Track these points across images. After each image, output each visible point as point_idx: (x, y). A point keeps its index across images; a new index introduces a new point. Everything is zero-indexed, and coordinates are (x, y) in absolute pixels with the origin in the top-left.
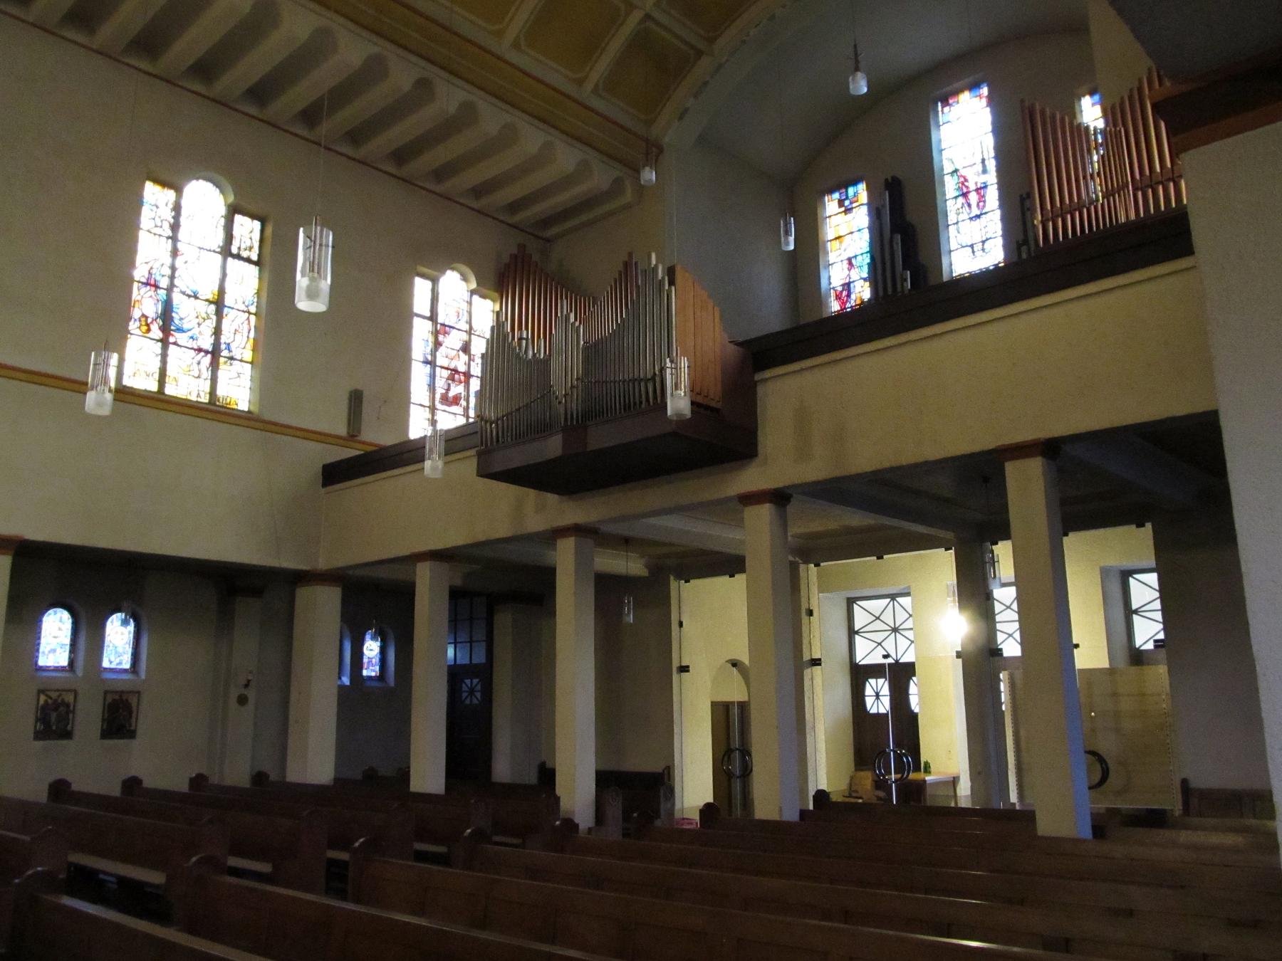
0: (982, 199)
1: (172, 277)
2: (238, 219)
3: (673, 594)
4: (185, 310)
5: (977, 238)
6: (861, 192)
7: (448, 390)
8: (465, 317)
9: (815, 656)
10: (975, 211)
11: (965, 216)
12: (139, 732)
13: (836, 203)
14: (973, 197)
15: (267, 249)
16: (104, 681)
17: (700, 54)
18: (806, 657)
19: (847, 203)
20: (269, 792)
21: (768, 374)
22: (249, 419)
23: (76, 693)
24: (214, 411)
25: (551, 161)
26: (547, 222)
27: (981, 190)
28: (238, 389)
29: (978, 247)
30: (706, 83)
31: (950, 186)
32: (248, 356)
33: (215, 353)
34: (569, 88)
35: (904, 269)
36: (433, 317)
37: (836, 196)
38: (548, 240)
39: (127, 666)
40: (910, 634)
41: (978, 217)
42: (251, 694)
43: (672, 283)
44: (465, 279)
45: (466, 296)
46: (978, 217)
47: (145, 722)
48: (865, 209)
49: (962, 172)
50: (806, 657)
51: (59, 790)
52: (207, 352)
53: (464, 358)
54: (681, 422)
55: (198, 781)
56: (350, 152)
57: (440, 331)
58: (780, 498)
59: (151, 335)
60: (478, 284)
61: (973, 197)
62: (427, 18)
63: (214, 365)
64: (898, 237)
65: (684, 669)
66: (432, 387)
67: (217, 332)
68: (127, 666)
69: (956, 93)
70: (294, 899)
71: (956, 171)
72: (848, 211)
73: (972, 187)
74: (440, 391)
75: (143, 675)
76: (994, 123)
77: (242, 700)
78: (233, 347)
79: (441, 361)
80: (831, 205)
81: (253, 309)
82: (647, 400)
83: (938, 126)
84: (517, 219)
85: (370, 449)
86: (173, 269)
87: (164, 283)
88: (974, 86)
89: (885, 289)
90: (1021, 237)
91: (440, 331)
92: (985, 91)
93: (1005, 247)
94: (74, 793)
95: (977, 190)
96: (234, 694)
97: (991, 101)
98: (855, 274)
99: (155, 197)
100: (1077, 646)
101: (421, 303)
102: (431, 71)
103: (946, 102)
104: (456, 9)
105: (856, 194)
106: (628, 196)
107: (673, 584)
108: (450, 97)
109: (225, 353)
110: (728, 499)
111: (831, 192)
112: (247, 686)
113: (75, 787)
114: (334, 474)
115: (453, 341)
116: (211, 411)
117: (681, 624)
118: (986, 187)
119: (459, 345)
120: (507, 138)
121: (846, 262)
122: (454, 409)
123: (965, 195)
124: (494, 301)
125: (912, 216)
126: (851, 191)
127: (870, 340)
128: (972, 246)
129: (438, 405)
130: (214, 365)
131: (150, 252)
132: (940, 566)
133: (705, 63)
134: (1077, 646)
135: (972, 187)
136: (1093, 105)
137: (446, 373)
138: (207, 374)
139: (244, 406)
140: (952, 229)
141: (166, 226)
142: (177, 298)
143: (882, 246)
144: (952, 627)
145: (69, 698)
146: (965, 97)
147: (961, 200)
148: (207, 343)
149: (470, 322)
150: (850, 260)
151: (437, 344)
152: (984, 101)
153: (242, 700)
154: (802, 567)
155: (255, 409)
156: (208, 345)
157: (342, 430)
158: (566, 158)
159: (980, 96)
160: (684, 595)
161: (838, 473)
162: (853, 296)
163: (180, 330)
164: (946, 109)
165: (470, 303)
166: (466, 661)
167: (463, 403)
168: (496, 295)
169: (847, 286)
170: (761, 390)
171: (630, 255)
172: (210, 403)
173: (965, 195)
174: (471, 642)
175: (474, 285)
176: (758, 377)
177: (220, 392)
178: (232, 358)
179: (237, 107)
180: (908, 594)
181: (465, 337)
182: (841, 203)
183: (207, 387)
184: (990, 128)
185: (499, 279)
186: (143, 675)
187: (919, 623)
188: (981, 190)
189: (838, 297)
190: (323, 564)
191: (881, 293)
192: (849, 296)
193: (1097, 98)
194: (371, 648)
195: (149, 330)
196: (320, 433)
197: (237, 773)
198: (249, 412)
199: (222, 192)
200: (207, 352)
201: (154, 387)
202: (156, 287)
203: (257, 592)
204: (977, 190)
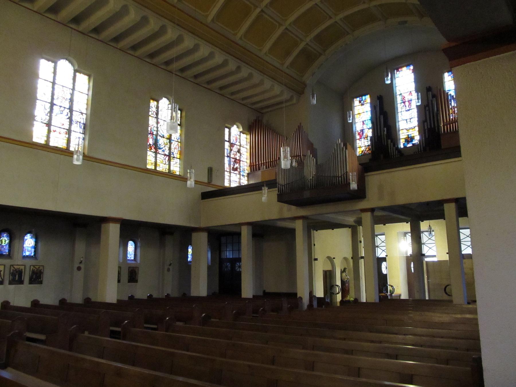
0: (410, 104)
1: (157, 131)
2: (77, 74)
3: (312, 234)
4: (162, 141)
5: (408, 118)
6: (367, 98)
7: (234, 166)
8: (238, 141)
9: (316, 257)
10: (408, 108)
11: (404, 109)
12: (139, 280)
13: (358, 102)
14: (407, 104)
15: (183, 120)
16: (128, 264)
17: (321, 54)
18: (360, 256)
19: (362, 102)
20: (89, 304)
21: (369, 174)
22: (56, 150)
23: (25, 266)
24: (170, 175)
25: (273, 90)
26: (262, 108)
27: (410, 101)
28: (176, 168)
29: (408, 121)
30: (322, 64)
31: (399, 99)
32: (178, 156)
33: (169, 156)
34: (277, 65)
35: (384, 127)
36: (229, 141)
37: (358, 99)
38: (263, 113)
39: (133, 258)
40: (384, 248)
41: (409, 110)
42: (171, 267)
43: (346, 149)
44: (238, 127)
45: (239, 133)
46: (409, 110)
47: (141, 276)
48: (369, 105)
49: (403, 95)
50: (360, 256)
51: (35, 303)
52: (167, 156)
53: (238, 154)
54: (354, 191)
55: (63, 302)
56: (180, 75)
57: (232, 145)
58: (372, 210)
59: (152, 150)
60: (78, 67)
61: (407, 104)
62: (221, 35)
63: (169, 160)
64: (382, 117)
65: (316, 259)
66: (230, 165)
67: (170, 149)
68: (133, 258)
69: (402, 67)
70: (120, 343)
71: (401, 94)
72: (362, 105)
73: (407, 100)
74: (232, 166)
75: (139, 262)
76: (415, 79)
77: (79, 269)
78: (174, 153)
79: (232, 156)
80: (356, 102)
81: (179, 141)
82: (342, 182)
83: (395, 78)
84: (254, 107)
85: (221, 188)
86: (157, 128)
87: (155, 133)
88: (408, 65)
89: (377, 133)
90: (424, 119)
91: (232, 145)
92: (412, 67)
93: (418, 121)
94: (42, 305)
95: (408, 101)
96: (166, 268)
97: (414, 71)
98: (365, 127)
99: (45, 67)
100: (447, 253)
102: (166, 22)
103: (398, 70)
104: (197, 10)
105: (365, 99)
106: (294, 101)
107: (312, 231)
108: (245, 72)
109: (172, 156)
110: (356, 210)
111: (357, 97)
112: (170, 265)
113: (41, 302)
114: (206, 196)
115: (235, 149)
117: (314, 245)
118: (411, 100)
119: (236, 150)
120: (261, 83)
121: (362, 123)
122: (236, 172)
123: (404, 102)
124: (246, 135)
125: (386, 108)
126: (364, 98)
127: (404, 166)
128: (406, 120)
129: (232, 171)
130: (169, 160)
131: (43, 90)
132: (406, 227)
133: (322, 58)
134: (447, 253)
135: (407, 100)
136: (449, 76)
137: (233, 160)
138: (167, 163)
139: (178, 173)
140: (399, 114)
141: (155, 113)
142: (159, 137)
143: (376, 119)
144: (405, 246)
145: (41, 268)
146: (404, 69)
147: (403, 104)
148: (167, 152)
149: (240, 142)
150: (363, 122)
151: (231, 150)
152: (411, 71)
153: (169, 270)
154: (358, 227)
155: (182, 174)
156: (167, 154)
157: (206, 180)
158: (277, 89)
159: (410, 69)
160: (315, 235)
161: (392, 204)
162: (364, 134)
163: (160, 149)
164: (398, 73)
165: (240, 136)
167: (239, 170)
168: (248, 133)
169: (362, 131)
170: (366, 179)
171: (301, 123)
172: (169, 172)
173: (404, 102)
174: (233, 250)
175: (241, 130)
176: (366, 174)
177: (172, 169)
178: (174, 157)
179: (69, 25)
180: (384, 235)
181: (238, 147)
182: (360, 102)
183: (167, 167)
184: (413, 80)
185: (249, 128)
186: (139, 262)
187: (395, 245)
188: (410, 101)
189: (359, 134)
190: (203, 225)
191: (376, 135)
192: (363, 134)
193: (450, 73)
194: (131, 247)
195: (151, 149)
196: (140, 169)
197: (77, 298)
198: (179, 175)
199: (72, 64)
200: (167, 156)
201: (153, 168)
202: (153, 134)
203: (172, 234)
204: (408, 101)
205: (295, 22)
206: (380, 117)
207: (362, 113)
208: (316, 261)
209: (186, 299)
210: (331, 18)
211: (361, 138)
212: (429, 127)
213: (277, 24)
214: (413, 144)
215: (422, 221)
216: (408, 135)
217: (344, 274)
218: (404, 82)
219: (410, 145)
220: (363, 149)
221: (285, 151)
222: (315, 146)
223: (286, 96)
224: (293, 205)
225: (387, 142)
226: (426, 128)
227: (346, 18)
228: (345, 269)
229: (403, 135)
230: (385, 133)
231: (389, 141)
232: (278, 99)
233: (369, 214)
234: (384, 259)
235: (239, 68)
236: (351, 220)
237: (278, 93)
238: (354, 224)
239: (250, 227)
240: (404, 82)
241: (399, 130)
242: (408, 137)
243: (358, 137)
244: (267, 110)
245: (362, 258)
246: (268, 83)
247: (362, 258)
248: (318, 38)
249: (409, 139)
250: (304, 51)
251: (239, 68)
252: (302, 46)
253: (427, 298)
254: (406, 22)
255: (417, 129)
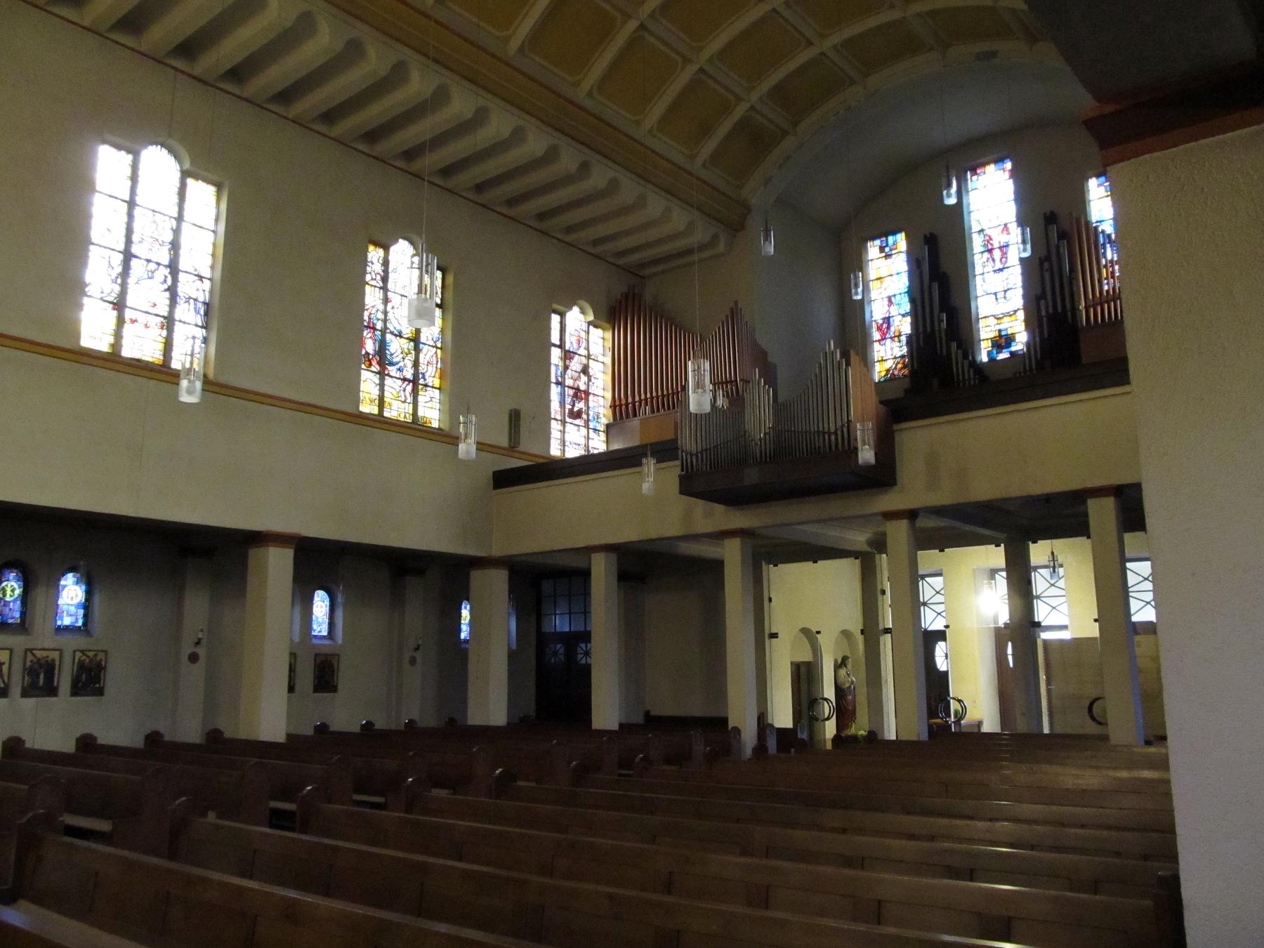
0: (1004, 255)
1: (385, 321)
2: (190, 181)
3: (764, 573)
4: (396, 346)
5: (1000, 288)
6: (900, 241)
7: (573, 406)
8: (584, 345)
9: (774, 631)
10: (998, 265)
11: (989, 268)
12: (339, 687)
13: (877, 249)
14: (997, 254)
15: (449, 294)
16: (314, 646)
17: (785, 133)
18: (881, 627)
19: (887, 249)
20: (218, 745)
21: (904, 425)
22: (138, 367)
23: (61, 651)
24: (416, 428)
25: (668, 220)
26: (643, 265)
27: (1004, 248)
28: (431, 411)
29: (1000, 295)
30: (789, 157)
31: (977, 243)
32: (437, 383)
33: (414, 382)
34: (680, 159)
35: (941, 311)
36: (561, 346)
37: (878, 242)
38: (643, 278)
39: (325, 633)
40: (940, 608)
41: (1001, 270)
42: (418, 655)
43: (848, 364)
45: (585, 326)
46: (1001, 270)
47: (345, 677)
48: (903, 257)
49: (988, 232)
50: (881, 627)
51: (86, 743)
52: (409, 381)
53: (584, 378)
54: (868, 468)
55: (153, 739)
56: (441, 183)
57: (568, 355)
58: (912, 515)
59: (373, 369)
60: (192, 164)
61: (997, 254)
62: (541, 85)
63: (415, 393)
64: (936, 286)
65: (774, 636)
66: (562, 404)
67: (416, 364)
68: (325, 633)
69: (984, 165)
71: (982, 231)
72: (888, 256)
73: (996, 245)
74: (568, 406)
75: (340, 641)
76: (1017, 193)
77: (194, 658)
78: (427, 375)
79: (569, 382)
80: (873, 249)
81: (439, 345)
83: (968, 192)
84: (621, 262)
85: (541, 461)
86: (385, 313)
87: (379, 325)
88: (999, 160)
89: (925, 326)
90: (1039, 292)
91: (568, 355)
92: (1008, 165)
93: (1024, 296)
94: (103, 746)
95: (1000, 248)
96: (407, 655)
97: (1014, 174)
98: (894, 311)
99: (109, 164)
100: (1096, 620)
101: (375, 267)
102: (407, 54)
103: (974, 172)
104: (482, 24)
105: (895, 243)
106: (721, 247)
107: (764, 567)
108: (600, 176)
109: (421, 381)
110: (872, 515)
111: (873, 239)
112: (417, 649)
113: (101, 741)
114: (504, 479)
115: (576, 364)
116: (380, 422)
117: (770, 600)
118: (1007, 246)
119: (579, 368)
120: (640, 203)
121: (886, 301)
122: (577, 422)
123: (990, 251)
124: (604, 329)
125: (946, 265)
126: (891, 239)
127: (990, 406)
128: (995, 294)
129: (568, 420)
130: (415, 393)
132: (995, 556)
133: (789, 143)
134: (1096, 620)
135: (996, 245)
136: (1099, 185)
137: (571, 392)
138: (410, 399)
139: (435, 425)
140: (979, 279)
141: (378, 278)
142: (389, 337)
143: (922, 291)
144: (992, 603)
145: (101, 656)
146: (991, 168)
147: (986, 255)
148: (409, 374)
149: (587, 349)
150: (889, 298)
151: (566, 368)
152: (1007, 175)
153: (413, 661)
154: (877, 556)
155: (445, 427)
156: (409, 376)
157: (504, 442)
158: (679, 218)
159: (1004, 170)
160: (772, 576)
161: (961, 500)
162: (892, 329)
163: (392, 364)
164: (975, 178)
165: (588, 333)
166: (567, 630)
167: (584, 416)
168: (608, 326)
169: (887, 320)
170: (897, 437)
171: (736, 302)
172: (413, 422)
173: (990, 251)
174: (570, 613)
175: (591, 318)
176: (895, 427)
177: (420, 413)
178: (426, 385)
179: (168, 62)
180: (940, 575)
181: (584, 361)
182: (882, 249)
183: (410, 409)
184: (1012, 197)
185: (611, 314)
186: (340, 641)
187: (967, 599)
188: (1004, 248)
189: (879, 328)
190: (497, 551)
191: (921, 330)
192: (888, 328)
193: (1103, 179)
194: (321, 604)
195: (371, 365)
196: (343, 413)
197: (190, 730)
198: (439, 429)
199: (177, 158)
200: (409, 381)
201: (375, 411)
202: (374, 329)
203: (420, 572)
204: (1000, 248)
205: (723, 54)
206: (930, 288)
207: (887, 277)
208: (774, 640)
209: (456, 732)
210: (810, 43)
211: (884, 338)
212: (1051, 311)
213: (680, 60)
214: (1011, 353)
215: (1035, 542)
216: (1000, 331)
217: (843, 672)
218: (991, 201)
219: (1004, 355)
220: (890, 364)
221: (697, 371)
222: (772, 358)
223: (700, 235)
224: (719, 502)
225: (949, 348)
226: (1044, 313)
227: (848, 43)
228: (845, 659)
229: (986, 332)
230: (944, 325)
231: (954, 345)
232: (681, 244)
233: (903, 524)
234: (941, 635)
235: (585, 167)
236: (859, 538)
237: (682, 228)
238: (866, 548)
239: (613, 557)
240: (991, 201)
241: (978, 319)
242: (1000, 336)
243: (876, 335)
244: (653, 270)
245: (887, 631)
246: (656, 204)
247: (887, 631)
248: (780, 93)
249: (1002, 341)
250: (744, 125)
251: (585, 167)
252: (739, 112)
253: (1046, 731)
254: (994, 54)
255: (1021, 315)
